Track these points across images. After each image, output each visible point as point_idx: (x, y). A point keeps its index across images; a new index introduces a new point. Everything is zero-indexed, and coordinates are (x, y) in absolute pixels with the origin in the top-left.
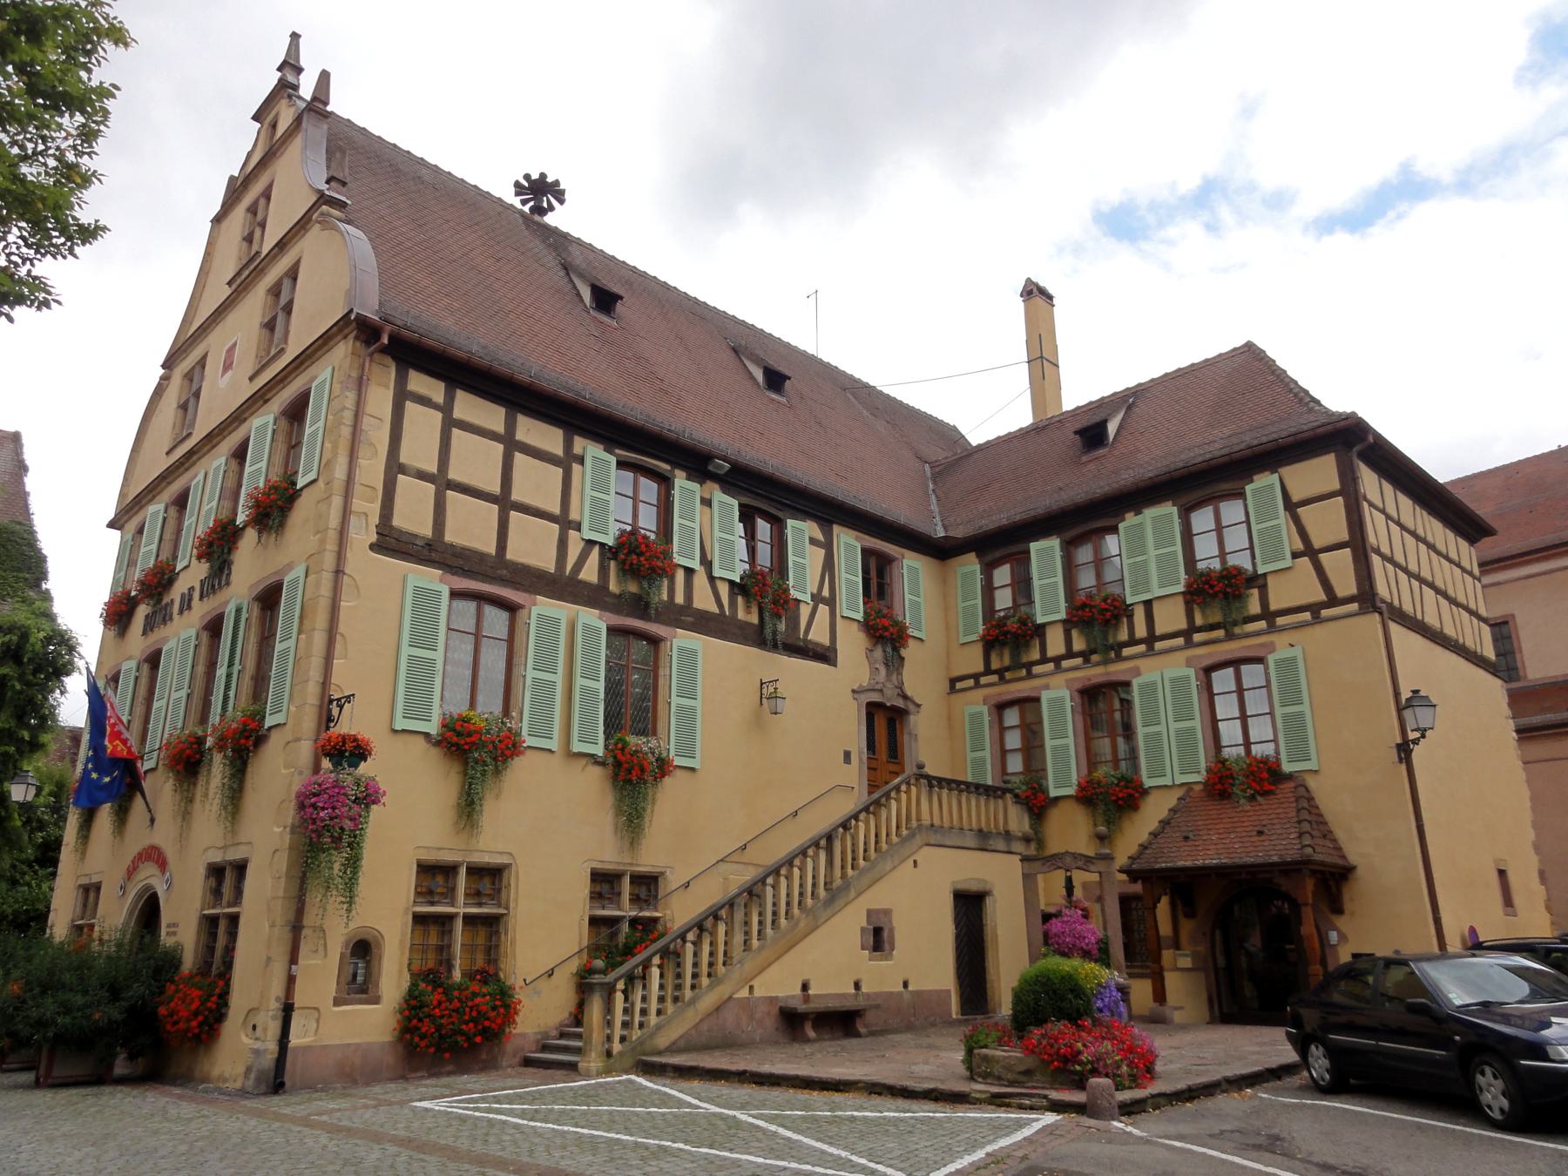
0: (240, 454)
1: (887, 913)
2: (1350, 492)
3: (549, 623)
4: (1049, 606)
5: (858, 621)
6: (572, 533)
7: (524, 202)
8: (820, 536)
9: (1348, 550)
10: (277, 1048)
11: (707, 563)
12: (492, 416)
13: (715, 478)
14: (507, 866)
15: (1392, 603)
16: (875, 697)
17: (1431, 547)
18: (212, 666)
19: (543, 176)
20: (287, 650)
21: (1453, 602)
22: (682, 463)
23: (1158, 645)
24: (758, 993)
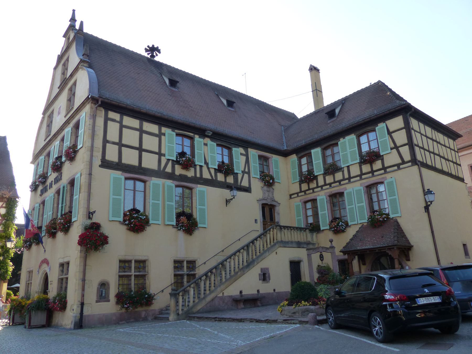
0: (63, 140)
1: (267, 269)
3: (156, 186)
4: (318, 170)
7: (148, 54)
8: (243, 152)
9: (407, 146)
11: (206, 163)
12: (135, 123)
13: (208, 137)
17: (439, 143)
19: (153, 46)
22: (197, 133)
23: (352, 180)
24: (225, 295)
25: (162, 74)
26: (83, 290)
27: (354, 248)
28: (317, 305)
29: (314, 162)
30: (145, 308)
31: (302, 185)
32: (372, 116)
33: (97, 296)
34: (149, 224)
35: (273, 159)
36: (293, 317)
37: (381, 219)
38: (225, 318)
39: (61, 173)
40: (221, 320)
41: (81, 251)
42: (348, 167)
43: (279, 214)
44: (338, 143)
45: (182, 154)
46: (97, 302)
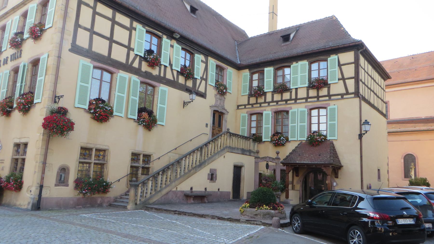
1: (215, 170)
2: (357, 63)
4: (268, 87)
5: (213, 86)
6: (131, 52)
8: (204, 60)
10: (38, 198)
11: (171, 65)
14: (108, 150)
15: (363, 96)
16: (216, 109)
17: (375, 81)
18: (15, 82)
20: (41, 80)
21: (378, 97)
22: (166, 33)
23: (298, 101)
26: (43, 172)
27: (293, 161)
28: (276, 210)
29: (265, 80)
30: (101, 195)
31: (251, 98)
32: (327, 47)
33: (56, 180)
34: (113, 116)
35: (228, 70)
36: (255, 219)
37: (319, 140)
38: (186, 213)
39: (21, 51)
40: (180, 213)
41: (44, 134)
42: (296, 89)
43: (226, 121)
44: (290, 66)
45: (150, 52)
46: (56, 185)
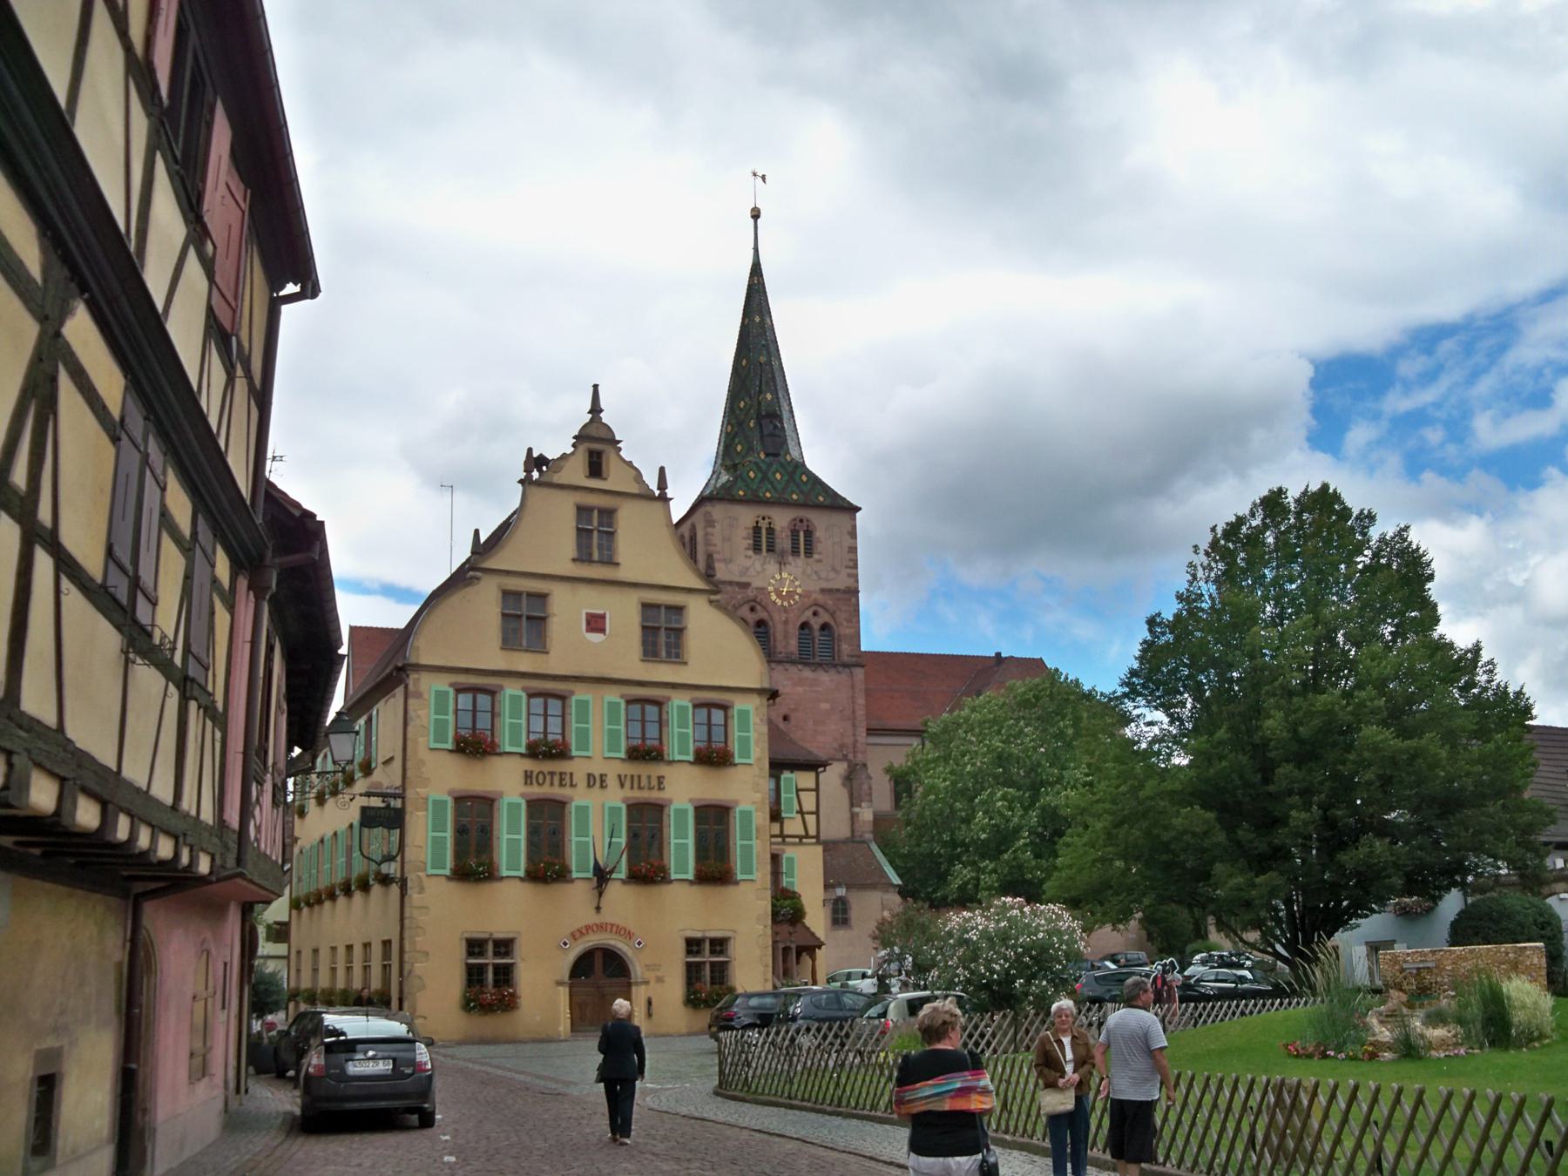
25: (1308, 1156)
